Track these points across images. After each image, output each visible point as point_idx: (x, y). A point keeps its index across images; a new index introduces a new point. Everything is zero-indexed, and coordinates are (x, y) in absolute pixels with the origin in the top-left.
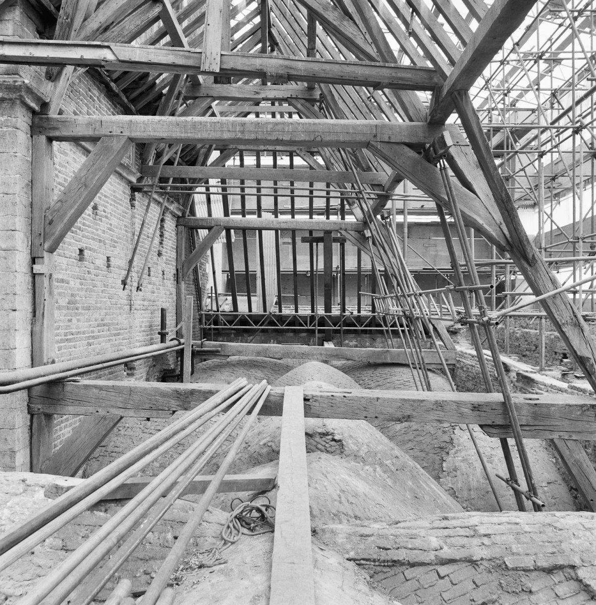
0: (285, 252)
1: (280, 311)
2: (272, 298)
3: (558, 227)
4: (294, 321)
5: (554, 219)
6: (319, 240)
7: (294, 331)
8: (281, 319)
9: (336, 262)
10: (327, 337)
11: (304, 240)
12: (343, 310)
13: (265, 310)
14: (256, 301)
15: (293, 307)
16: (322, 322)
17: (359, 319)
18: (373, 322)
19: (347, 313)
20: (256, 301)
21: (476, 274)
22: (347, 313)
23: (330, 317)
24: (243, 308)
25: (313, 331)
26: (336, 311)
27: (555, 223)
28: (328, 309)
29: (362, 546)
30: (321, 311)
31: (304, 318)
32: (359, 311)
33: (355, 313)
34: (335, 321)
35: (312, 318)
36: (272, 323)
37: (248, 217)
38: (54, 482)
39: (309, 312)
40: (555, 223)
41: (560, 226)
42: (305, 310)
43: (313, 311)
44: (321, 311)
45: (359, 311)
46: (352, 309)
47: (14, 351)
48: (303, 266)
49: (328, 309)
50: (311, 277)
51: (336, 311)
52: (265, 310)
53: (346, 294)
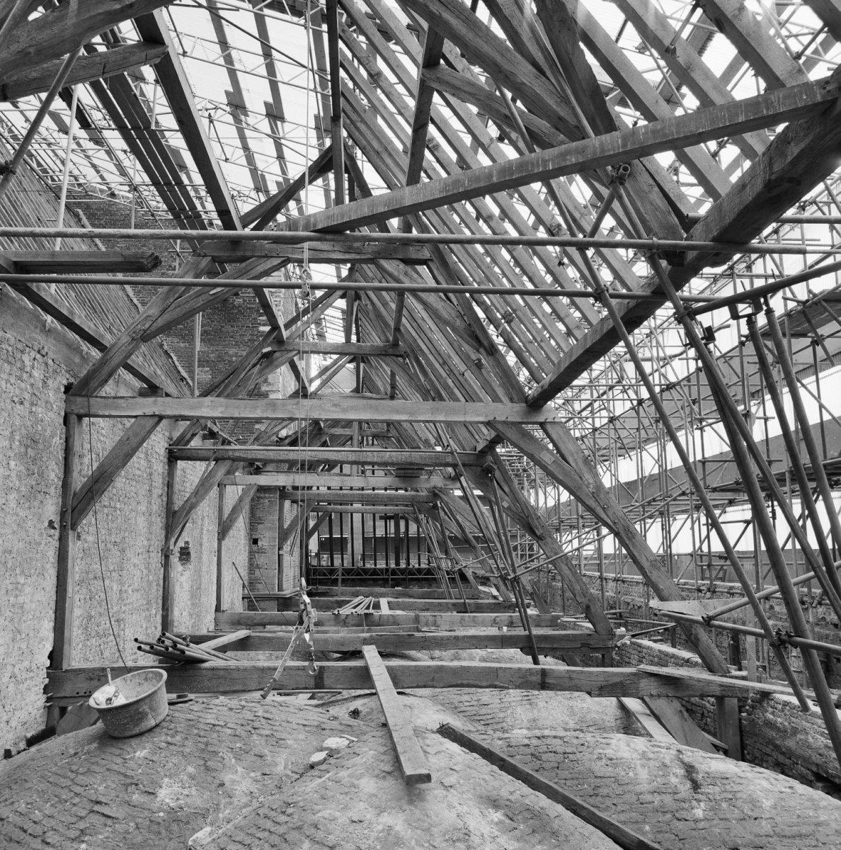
0: (369, 523)
1: (364, 565)
2: (358, 557)
3: (832, 416)
4: (375, 572)
5: (823, 401)
6: (390, 518)
7: (373, 580)
8: (366, 571)
9: (402, 529)
10: (397, 583)
11: (381, 518)
12: (408, 564)
13: (353, 565)
14: (347, 557)
15: (372, 562)
16: (394, 572)
17: (419, 571)
18: (429, 572)
19: (411, 567)
20: (347, 557)
21: (472, 539)
22: (411, 567)
23: (399, 569)
24: (337, 562)
25: (387, 579)
26: (403, 565)
27: (828, 411)
28: (397, 563)
29: (465, 808)
30: (393, 566)
31: (381, 570)
32: (419, 565)
33: (417, 566)
34: (403, 571)
35: (387, 570)
36: (359, 574)
37: (376, 491)
38: (305, 762)
39: (384, 566)
40: (828, 411)
41: (836, 415)
42: (381, 565)
43: (387, 564)
44: (393, 566)
45: (419, 565)
46: (414, 563)
47: (424, 786)
48: (380, 533)
49: (397, 563)
50: (385, 539)
51: (403, 565)
52: (353, 565)
53: (411, 551)
